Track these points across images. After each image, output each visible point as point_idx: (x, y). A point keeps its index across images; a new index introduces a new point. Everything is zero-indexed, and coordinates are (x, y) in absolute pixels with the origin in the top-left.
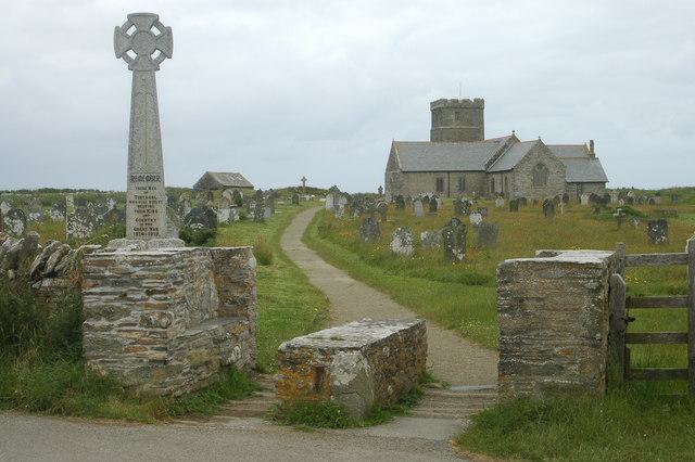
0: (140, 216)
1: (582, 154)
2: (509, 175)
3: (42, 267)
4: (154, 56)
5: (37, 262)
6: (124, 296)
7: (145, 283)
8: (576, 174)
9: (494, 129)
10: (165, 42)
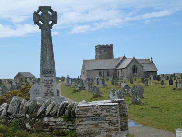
0: (46, 88)
1: (148, 62)
2: (124, 70)
3: (44, 112)
4: (40, 22)
5: (40, 110)
6: (97, 125)
7: (107, 118)
8: (147, 69)
9: (117, 54)
10: (54, 17)
